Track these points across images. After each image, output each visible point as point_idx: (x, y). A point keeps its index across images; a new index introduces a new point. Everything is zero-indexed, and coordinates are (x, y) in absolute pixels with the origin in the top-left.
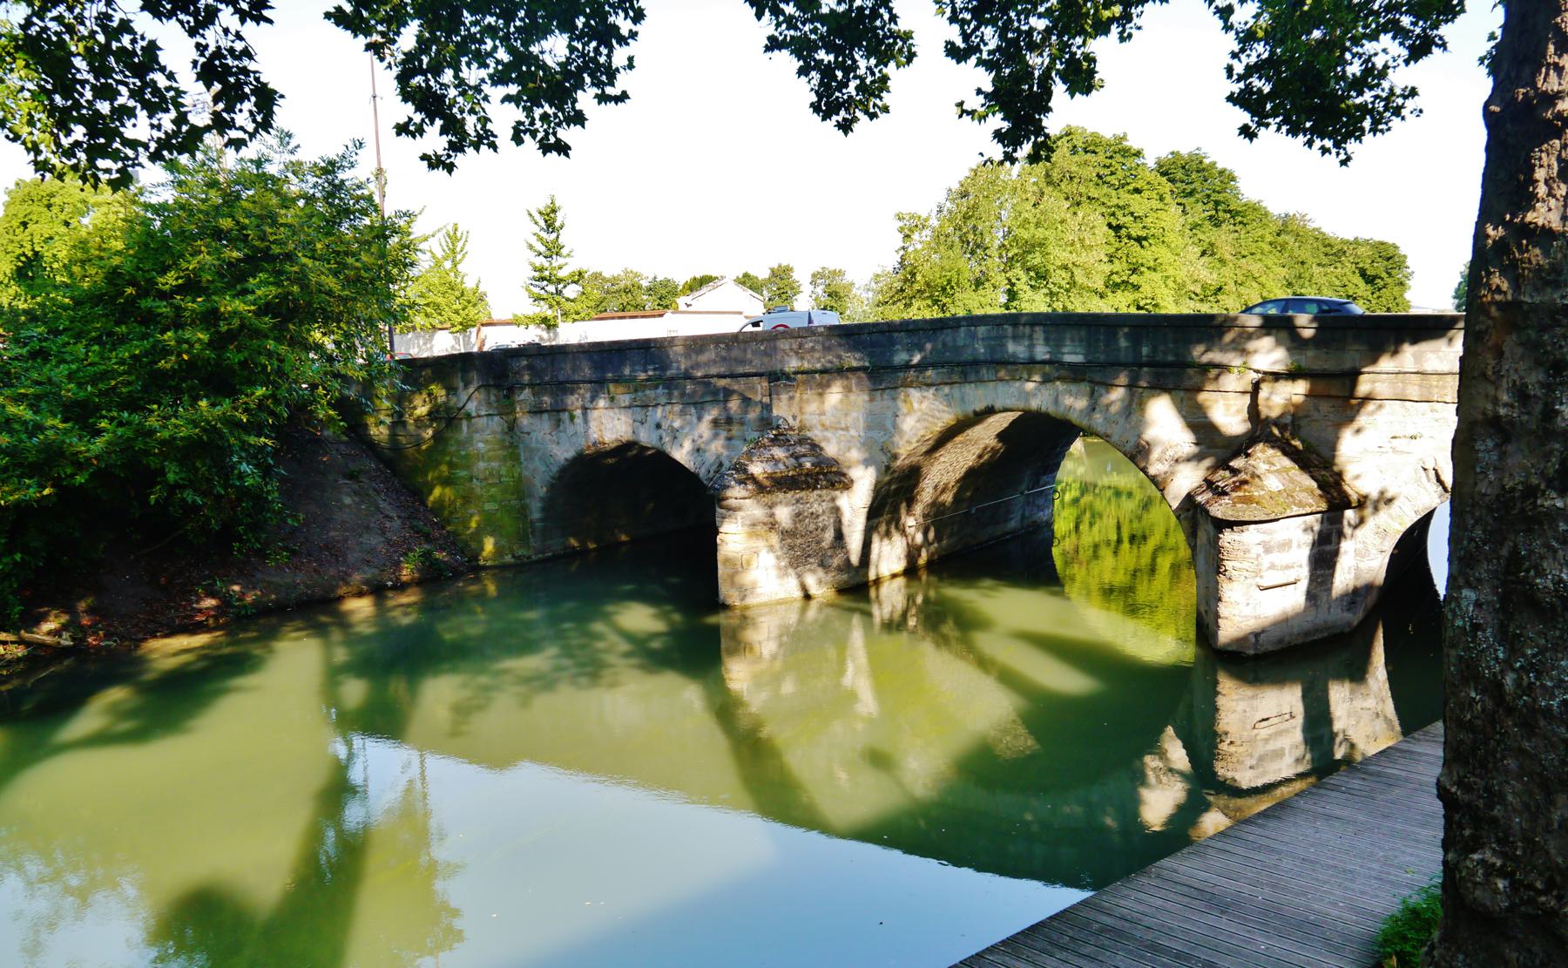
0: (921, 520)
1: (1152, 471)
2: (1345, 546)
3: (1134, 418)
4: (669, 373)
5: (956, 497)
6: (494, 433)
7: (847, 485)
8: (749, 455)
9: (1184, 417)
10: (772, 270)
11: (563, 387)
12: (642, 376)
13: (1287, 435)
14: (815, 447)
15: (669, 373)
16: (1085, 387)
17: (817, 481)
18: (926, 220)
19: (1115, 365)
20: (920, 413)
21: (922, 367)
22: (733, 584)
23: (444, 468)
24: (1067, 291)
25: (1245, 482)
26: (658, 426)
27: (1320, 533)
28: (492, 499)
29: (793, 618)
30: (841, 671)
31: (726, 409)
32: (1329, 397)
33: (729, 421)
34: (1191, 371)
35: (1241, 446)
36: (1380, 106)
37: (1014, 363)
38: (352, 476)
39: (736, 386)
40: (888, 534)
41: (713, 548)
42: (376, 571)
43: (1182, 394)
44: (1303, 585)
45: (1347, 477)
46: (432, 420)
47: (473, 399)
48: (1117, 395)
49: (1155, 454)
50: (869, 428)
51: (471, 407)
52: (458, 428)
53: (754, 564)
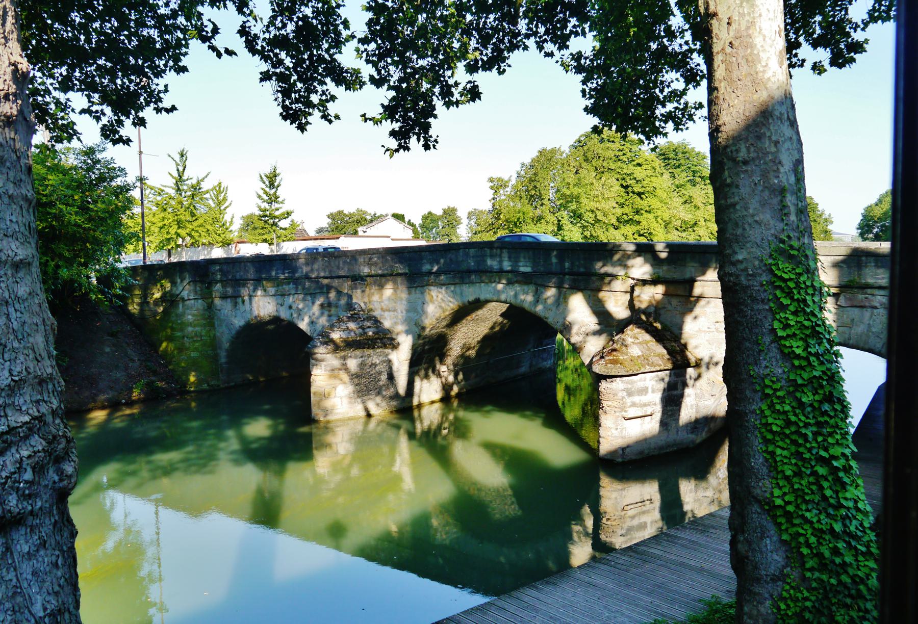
0: (451, 367)
1: (574, 340)
2: (688, 391)
3: (561, 308)
4: (297, 275)
5: (477, 352)
6: (198, 310)
7: (395, 347)
8: (332, 327)
9: (591, 307)
10: (444, 210)
11: (239, 283)
12: (282, 277)
13: (651, 319)
14: (377, 322)
15: (297, 275)
16: (532, 288)
17: (375, 343)
18: (506, 182)
19: (549, 274)
20: (438, 303)
21: (438, 274)
22: (319, 407)
23: (169, 331)
24: (593, 225)
25: (615, 350)
26: (290, 307)
27: (669, 383)
28: (196, 350)
29: (360, 427)
30: (392, 461)
31: (328, 298)
32: (677, 295)
33: (330, 305)
34: (594, 278)
35: (621, 326)
36: (679, 114)
37: (491, 272)
38: (113, 335)
39: (336, 283)
40: (427, 376)
41: (308, 384)
42: (116, 394)
43: (589, 292)
44: (658, 416)
45: (690, 347)
46: (163, 302)
47: (186, 289)
48: (551, 292)
49: (575, 330)
50: (408, 311)
51: (185, 294)
52: (177, 306)
53: (333, 395)
